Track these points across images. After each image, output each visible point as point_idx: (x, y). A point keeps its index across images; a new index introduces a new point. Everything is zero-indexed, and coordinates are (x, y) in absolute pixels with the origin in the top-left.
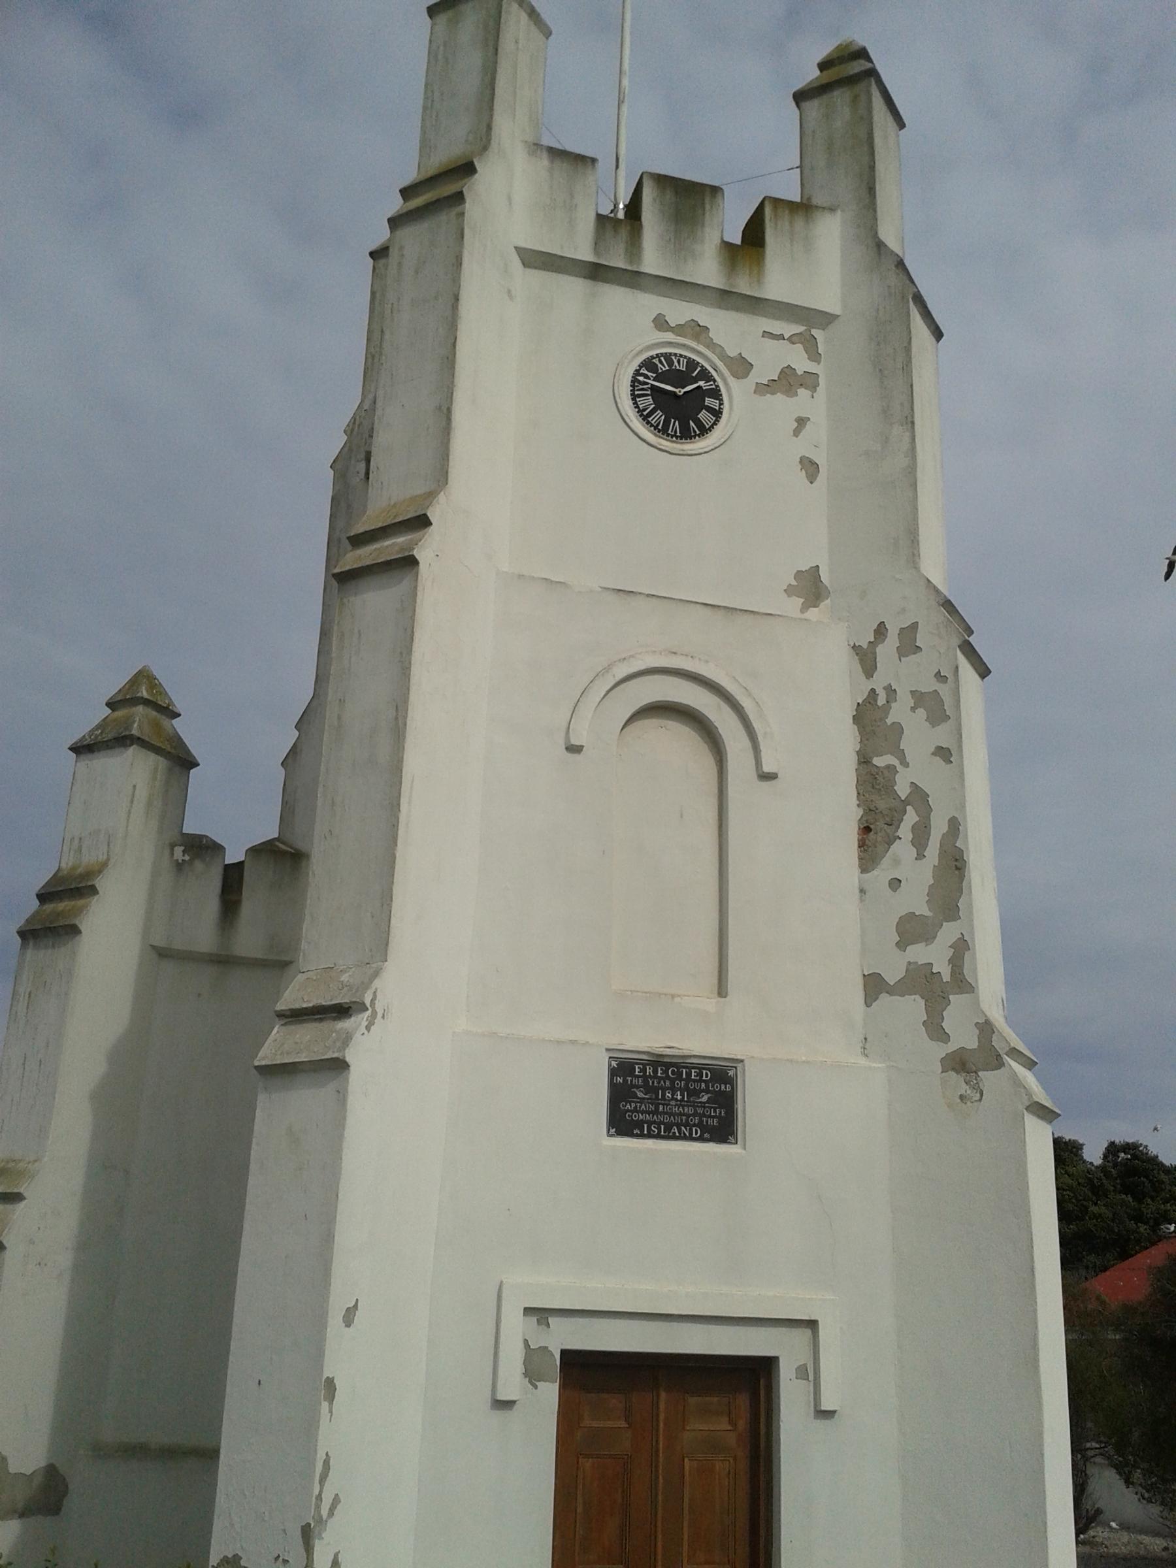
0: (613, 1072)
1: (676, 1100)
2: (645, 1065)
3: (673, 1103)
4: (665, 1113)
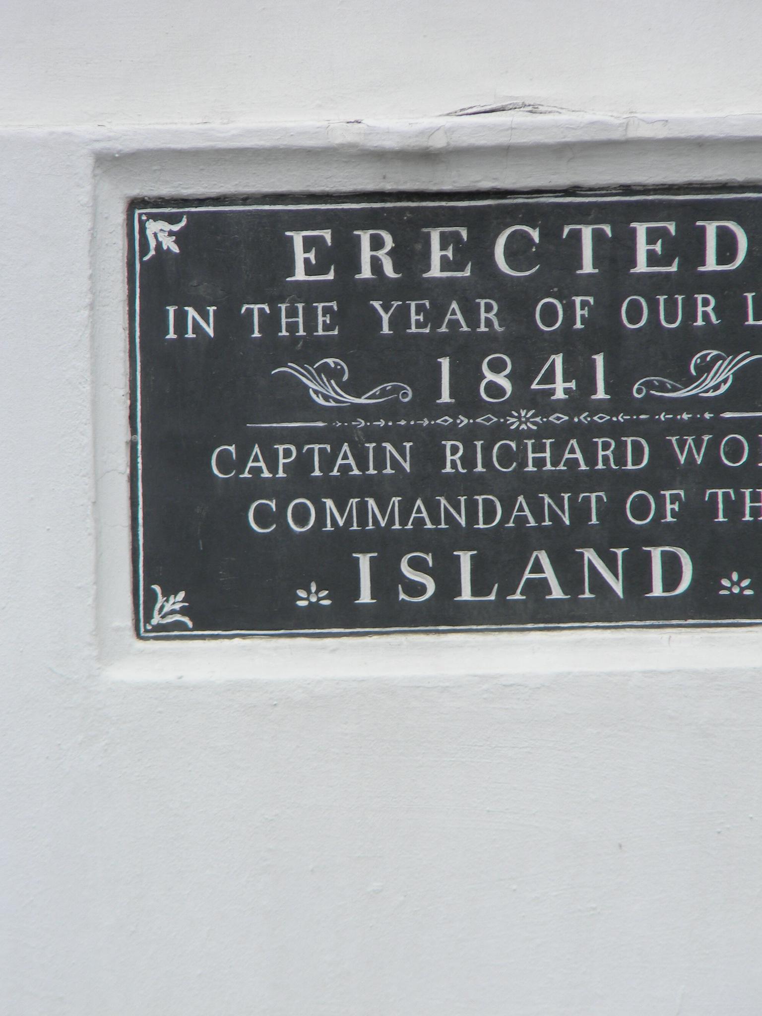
0: (155, 284)
1: (542, 403)
2: (345, 226)
3: (524, 420)
4: (469, 484)
